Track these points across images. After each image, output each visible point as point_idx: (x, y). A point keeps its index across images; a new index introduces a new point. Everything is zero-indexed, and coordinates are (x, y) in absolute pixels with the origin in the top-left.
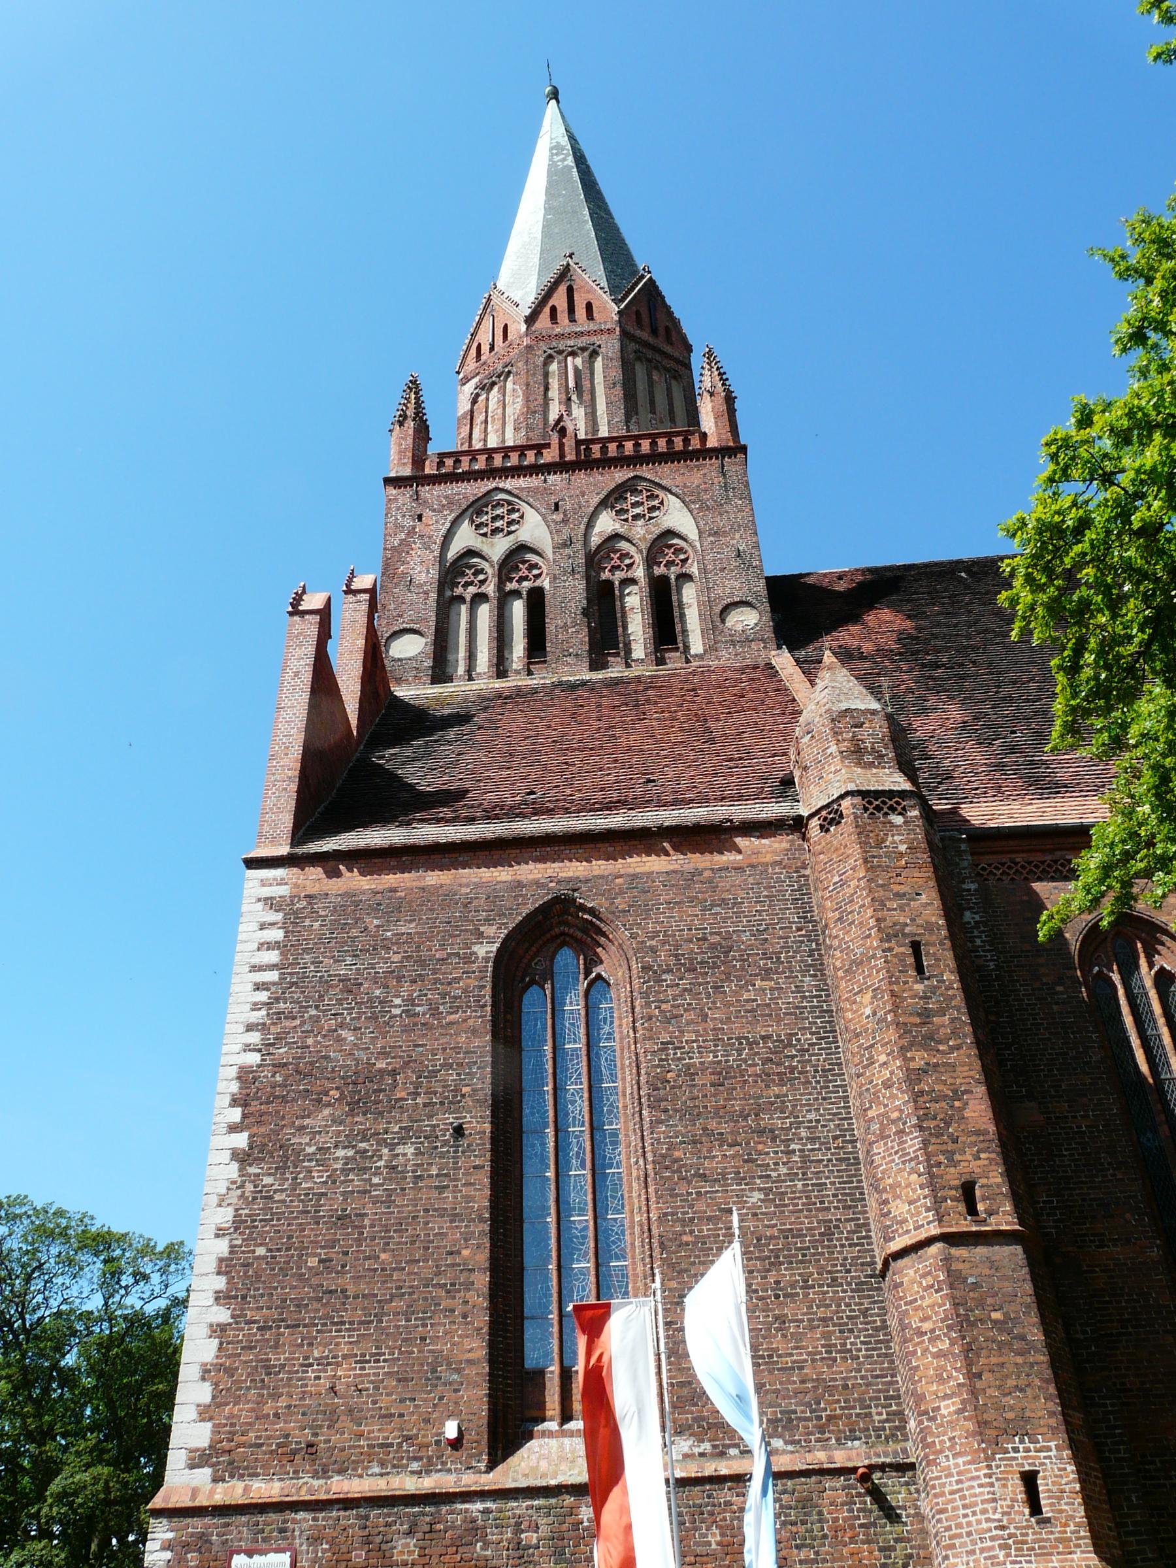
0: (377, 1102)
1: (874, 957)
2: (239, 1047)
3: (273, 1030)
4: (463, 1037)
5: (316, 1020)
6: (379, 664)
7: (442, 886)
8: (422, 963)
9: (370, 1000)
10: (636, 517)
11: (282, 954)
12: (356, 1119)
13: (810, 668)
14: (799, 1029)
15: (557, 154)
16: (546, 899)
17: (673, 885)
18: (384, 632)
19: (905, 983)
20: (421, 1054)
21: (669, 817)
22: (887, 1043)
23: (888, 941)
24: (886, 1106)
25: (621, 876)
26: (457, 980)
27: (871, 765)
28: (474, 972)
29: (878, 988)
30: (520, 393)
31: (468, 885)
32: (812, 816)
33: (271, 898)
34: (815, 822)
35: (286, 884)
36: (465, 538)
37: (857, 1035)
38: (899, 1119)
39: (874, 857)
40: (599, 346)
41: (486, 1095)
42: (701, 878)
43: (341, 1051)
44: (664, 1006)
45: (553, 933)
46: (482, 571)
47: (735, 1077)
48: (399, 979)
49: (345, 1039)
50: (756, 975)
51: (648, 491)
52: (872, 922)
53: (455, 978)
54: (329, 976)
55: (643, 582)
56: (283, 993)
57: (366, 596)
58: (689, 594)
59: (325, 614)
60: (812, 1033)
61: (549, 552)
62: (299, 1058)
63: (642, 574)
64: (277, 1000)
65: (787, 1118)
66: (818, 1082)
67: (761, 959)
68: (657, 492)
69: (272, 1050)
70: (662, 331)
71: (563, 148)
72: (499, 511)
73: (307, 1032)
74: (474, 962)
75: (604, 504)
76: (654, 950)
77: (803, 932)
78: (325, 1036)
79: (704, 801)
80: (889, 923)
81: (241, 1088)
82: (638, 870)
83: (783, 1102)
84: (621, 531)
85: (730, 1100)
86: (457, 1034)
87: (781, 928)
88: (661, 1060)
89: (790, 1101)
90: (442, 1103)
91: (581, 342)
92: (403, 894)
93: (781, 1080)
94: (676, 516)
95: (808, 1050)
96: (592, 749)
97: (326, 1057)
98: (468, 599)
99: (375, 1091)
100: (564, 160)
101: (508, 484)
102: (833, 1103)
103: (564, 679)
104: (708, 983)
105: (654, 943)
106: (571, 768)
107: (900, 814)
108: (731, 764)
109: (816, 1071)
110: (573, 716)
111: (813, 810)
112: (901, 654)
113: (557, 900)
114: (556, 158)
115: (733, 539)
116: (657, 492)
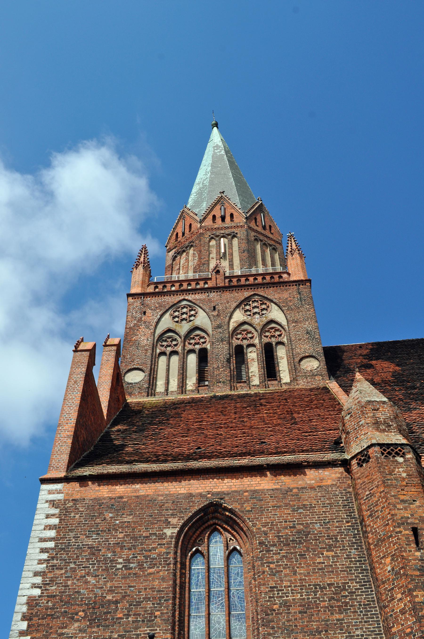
0: (106, 620)
1: (391, 536)
2: (28, 585)
3: (50, 575)
4: (156, 583)
5: (73, 570)
6: (120, 384)
7: (148, 495)
8: (135, 538)
9: (105, 559)
10: (255, 314)
11: (57, 532)
12: (94, 630)
13: (347, 388)
14: (349, 580)
15: (217, 149)
16: (205, 504)
17: (276, 497)
18: (123, 368)
19: (410, 551)
20: (132, 592)
21: (274, 459)
22: (401, 587)
23: (399, 527)
24: (402, 625)
25: (247, 491)
26: (154, 549)
27: (384, 431)
28: (164, 544)
29: (394, 555)
30: (197, 255)
31: (162, 495)
32: (353, 458)
33: (54, 501)
34: (354, 462)
35: (62, 493)
36: (167, 322)
37: (384, 583)
38: (411, 633)
39: (388, 480)
40: (237, 233)
41: (169, 616)
42: (291, 493)
43: (87, 589)
44: (272, 566)
45: (209, 523)
46: (175, 340)
47: (313, 608)
48: (122, 547)
49: (90, 582)
50: (324, 548)
51: (261, 301)
52: (389, 517)
53: (153, 548)
54: (83, 545)
55: (258, 346)
56: (57, 554)
57: (115, 348)
58: (281, 353)
59: (92, 352)
60: (356, 583)
61: (210, 331)
62: (63, 592)
63: (258, 342)
64: (53, 558)
65: (344, 633)
66: (361, 612)
67: (326, 539)
68: (265, 302)
69: (47, 587)
70: (268, 227)
71: (220, 147)
72: (185, 310)
73: (68, 577)
74: (164, 539)
75: (238, 307)
76: (266, 533)
77: (350, 524)
78: (78, 580)
79: (293, 452)
80: (398, 517)
81: (28, 609)
82: (256, 488)
83: (341, 624)
84: (247, 320)
85: (311, 622)
86: (153, 580)
87: (337, 522)
88: (270, 597)
89: (345, 623)
90: (143, 621)
91: (227, 231)
92: (126, 500)
93: (340, 610)
94: (276, 314)
95: (355, 593)
96: (232, 427)
97: (78, 592)
98: (168, 353)
99: (105, 613)
100: (220, 152)
101: (190, 297)
102: (371, 625)
103: (217, 394)
104: (297, 552)
105: (265, 529)
106: (220, 437)
107: (401, 456)
108: (307, 434)
109: (360, 605)
110: (221, 412)
111: (353, 455)
112: (394, 382)
113: (211, 504)
114: (216, 151)
115: (305, 324)
116: (265, 302)
